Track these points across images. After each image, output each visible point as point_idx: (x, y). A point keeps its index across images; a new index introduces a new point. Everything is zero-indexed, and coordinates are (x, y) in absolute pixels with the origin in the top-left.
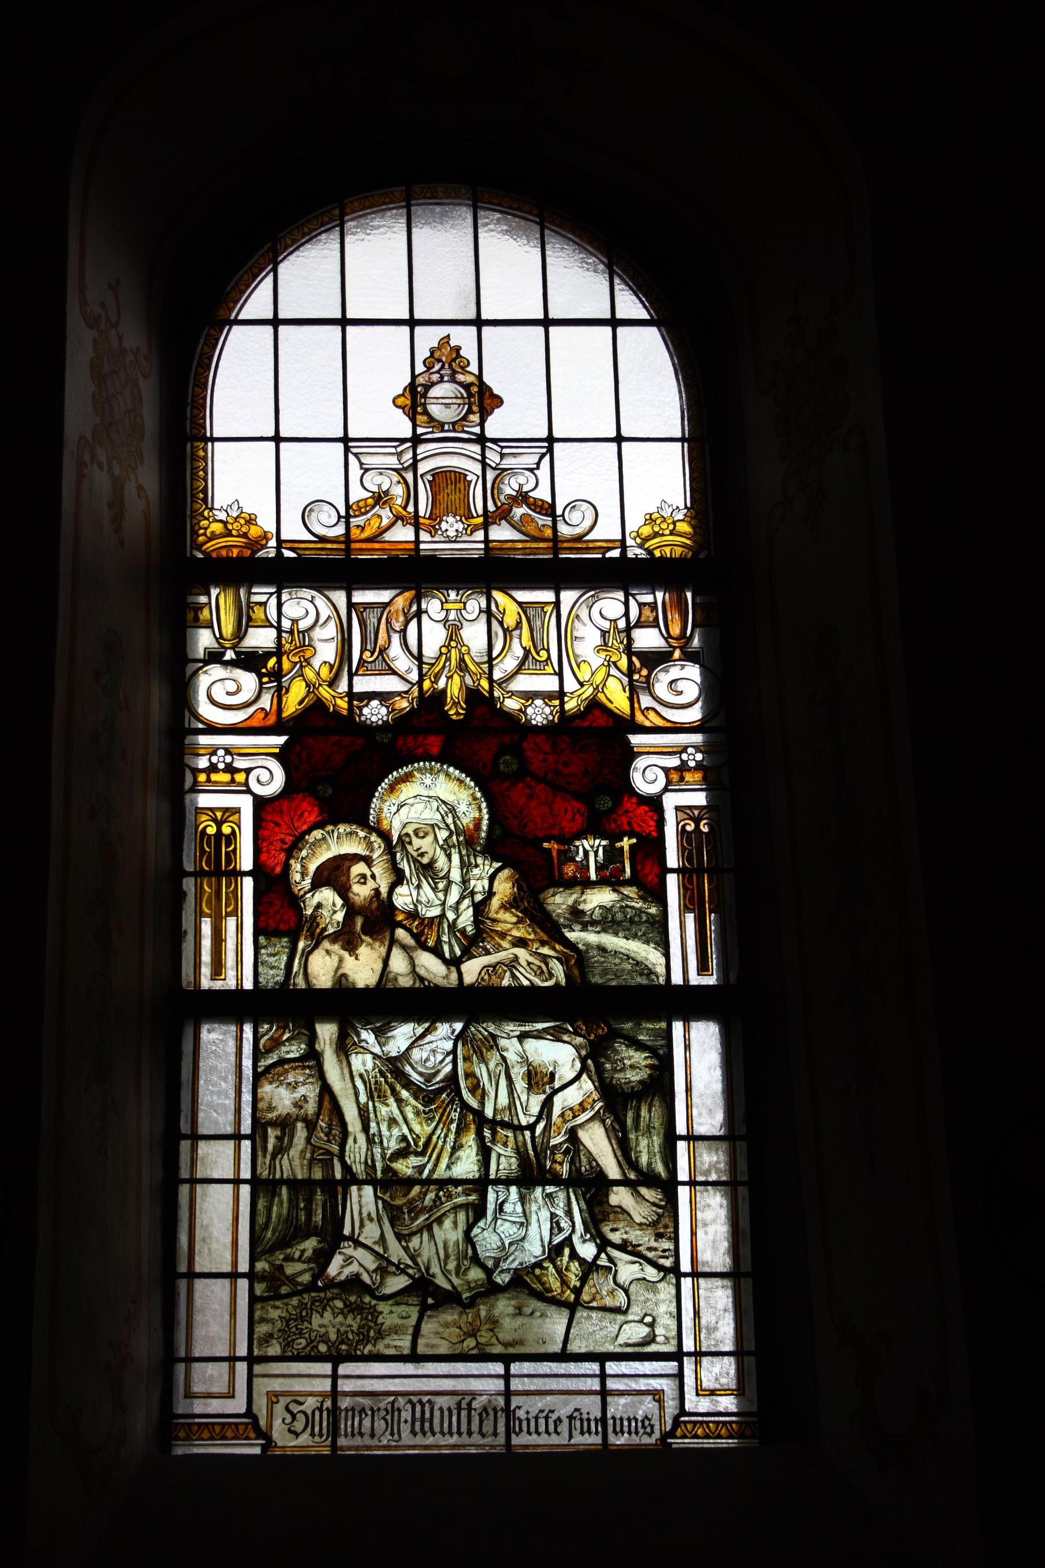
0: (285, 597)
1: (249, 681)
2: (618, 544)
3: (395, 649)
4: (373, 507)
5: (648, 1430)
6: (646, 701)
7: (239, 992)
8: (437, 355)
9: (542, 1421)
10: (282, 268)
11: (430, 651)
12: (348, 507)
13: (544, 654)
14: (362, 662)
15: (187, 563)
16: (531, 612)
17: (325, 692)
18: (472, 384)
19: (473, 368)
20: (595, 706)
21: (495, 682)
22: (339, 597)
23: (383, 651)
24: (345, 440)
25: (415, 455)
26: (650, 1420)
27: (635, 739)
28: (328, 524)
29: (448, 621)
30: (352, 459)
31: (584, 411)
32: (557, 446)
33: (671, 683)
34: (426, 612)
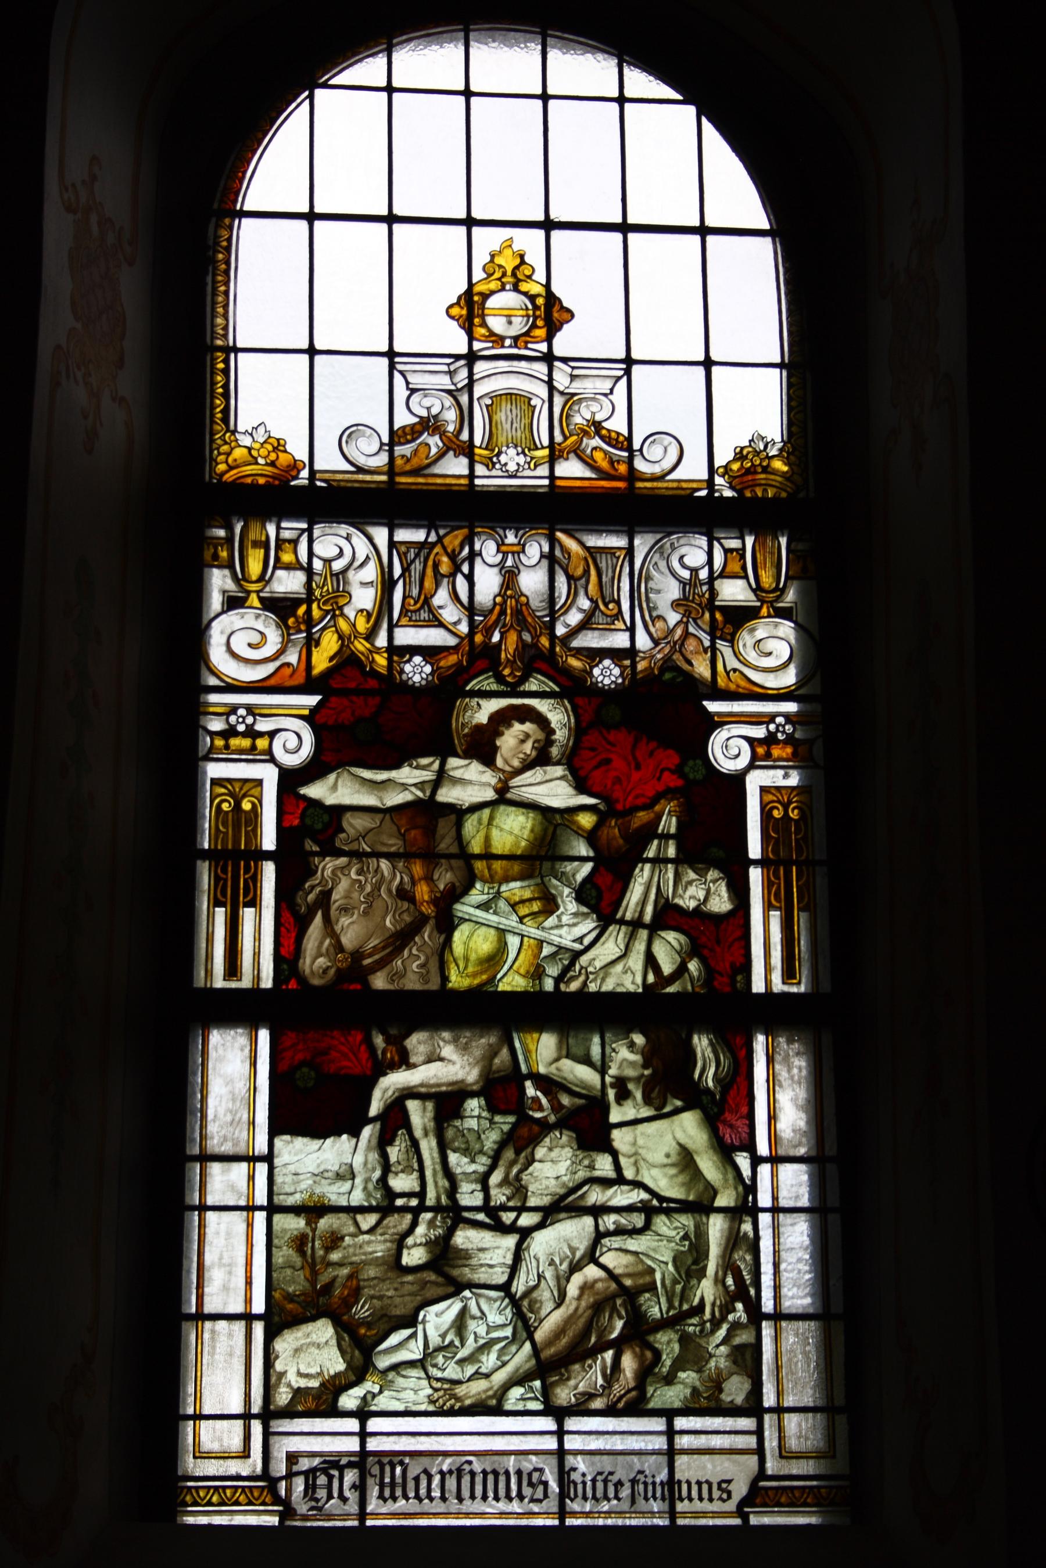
0: (316, 533)
2: (705, 485)
3: (441, 597)
7: (256, 992)
8: (498, 260)
9: (600, 1485)
12: (392, 432)
17: (360, 646)
19: (540, 276)
21: (558, 637)
22: (381, 535)
24: (391, 354)
25: (471, 374)
27: (713, 707)
28: (368, 451)
30: (398, 378)
31: (667, 327)
32: (635, 369)
34: (480, 554)
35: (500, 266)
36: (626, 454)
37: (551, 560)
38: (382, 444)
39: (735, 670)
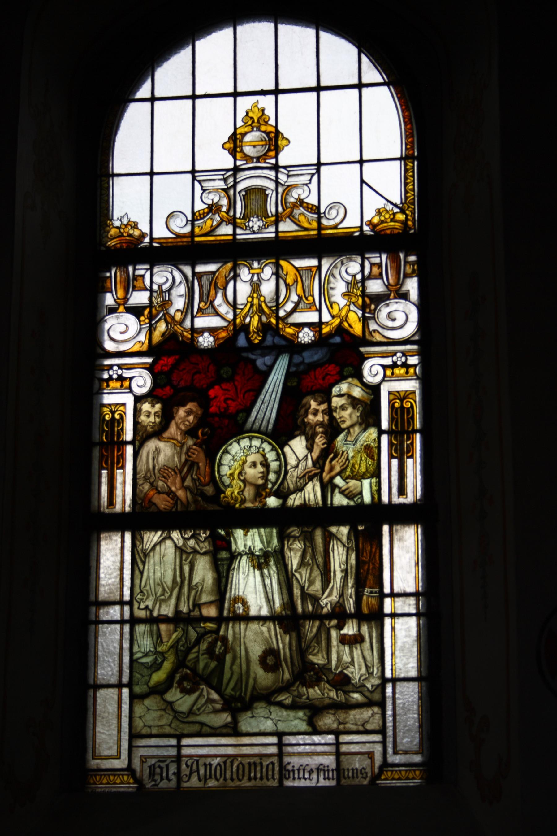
3: (219, 300)
6: (373, 326)
7: (123, 514)
8: (251, 114)
11: (242, 299)
12: (193, 213)
13: (310, 298)
14: (200, 309)
15: (100, 253)
18: (271, 132)
19: (272, 122)
20: (340, 330)
22: (188, 270)
28: (181, 226)
29: (252, 281)
31: (340, 144)
32: (323, 168)
33: (389, 313)
35: (251, 118)
36: (316, 216)
37: (277, 275)
38: (187, 221)
39: (375, 331)
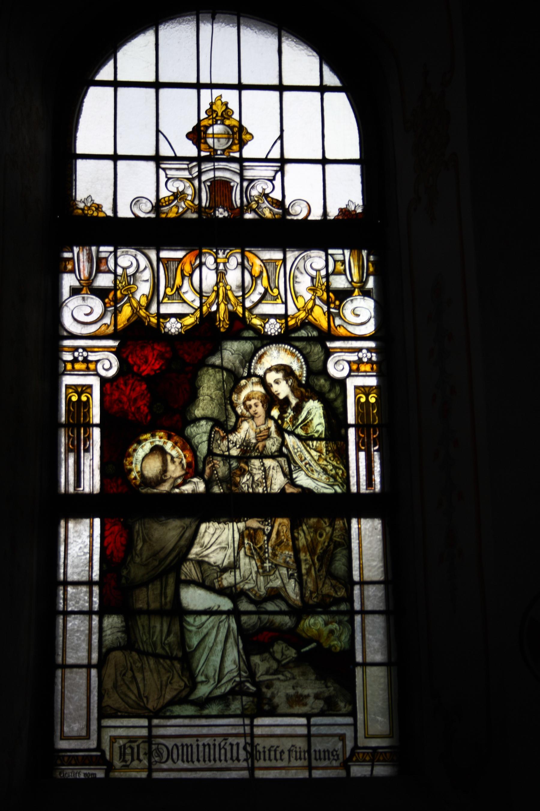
1: (97, 304)
3: (186, 287)
4: (173, 201)
5: (336, 757)
9: (272, 753)
10: (120, 55)
13: (276, 291)
16: (271, 268)
17: (142, 313)
18: (234, 126)
19: (236, 116)
23: (179, 288)
26: (337, 751)
28: (144, 211)
30: (161, 172)
